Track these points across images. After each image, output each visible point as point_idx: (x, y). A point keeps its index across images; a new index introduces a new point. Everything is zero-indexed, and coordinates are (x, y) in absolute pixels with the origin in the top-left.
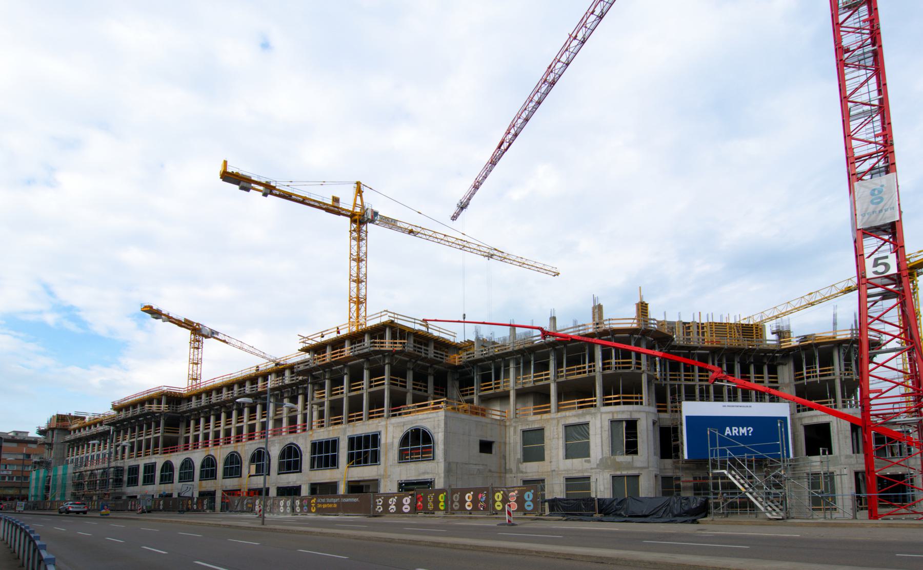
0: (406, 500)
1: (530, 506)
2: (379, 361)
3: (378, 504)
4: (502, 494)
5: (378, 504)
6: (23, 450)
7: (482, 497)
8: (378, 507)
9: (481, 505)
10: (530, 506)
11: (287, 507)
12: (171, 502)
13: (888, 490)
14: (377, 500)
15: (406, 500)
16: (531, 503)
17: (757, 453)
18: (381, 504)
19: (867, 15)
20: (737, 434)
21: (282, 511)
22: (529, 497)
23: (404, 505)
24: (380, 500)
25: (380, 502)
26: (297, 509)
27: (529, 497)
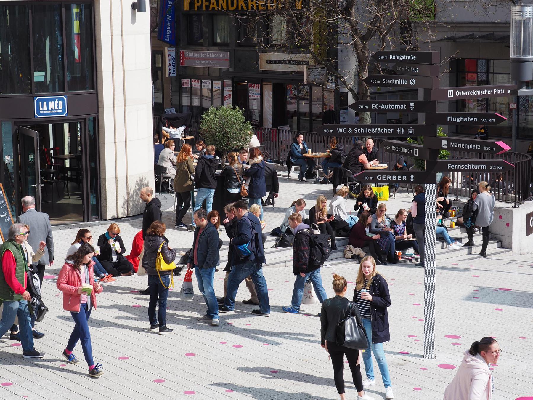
20: (390, 179)
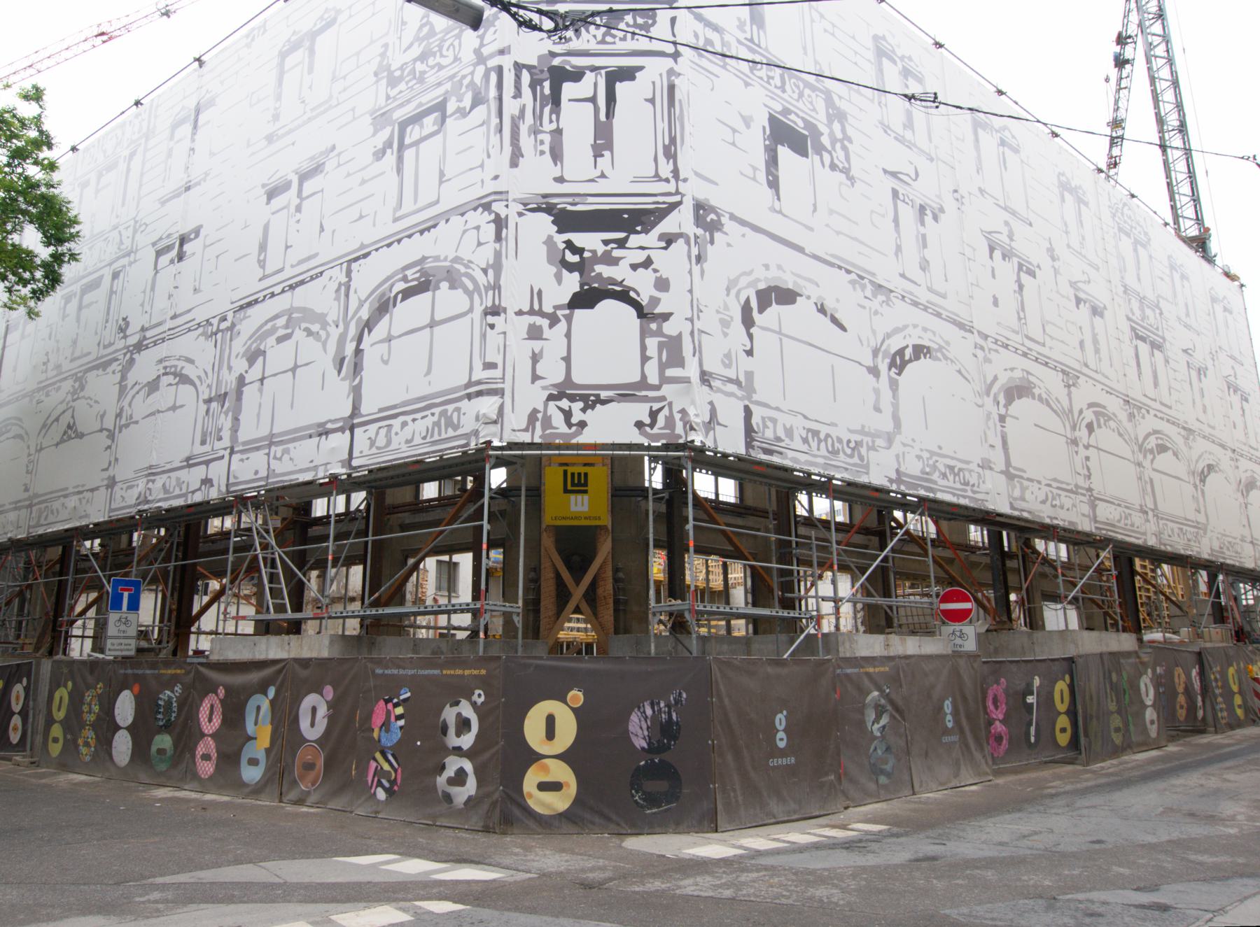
0: (551, 720)
1: (555, 787)
2: (798, 630)
3: (453, 740)
4: (221, 701)
5: (453, 740)
6: (656, 647)
7: (386, 725)
8: (453, 764)
9: (379, 772)
10: (555, 787)
11: (82, 725)
12: (780, 720)
13: (469, 516)
14: (449, 715)
15: (551, 720)
16: (562, 773)
17: (461, 523)
18: (467, 741)
19: (725, 567)
21: (782, 745)
22: (550, 734)
23: (535, 757)
24: (466, 710)
25: (464, 725)
26: (201, 750)
27: (550, 734)
